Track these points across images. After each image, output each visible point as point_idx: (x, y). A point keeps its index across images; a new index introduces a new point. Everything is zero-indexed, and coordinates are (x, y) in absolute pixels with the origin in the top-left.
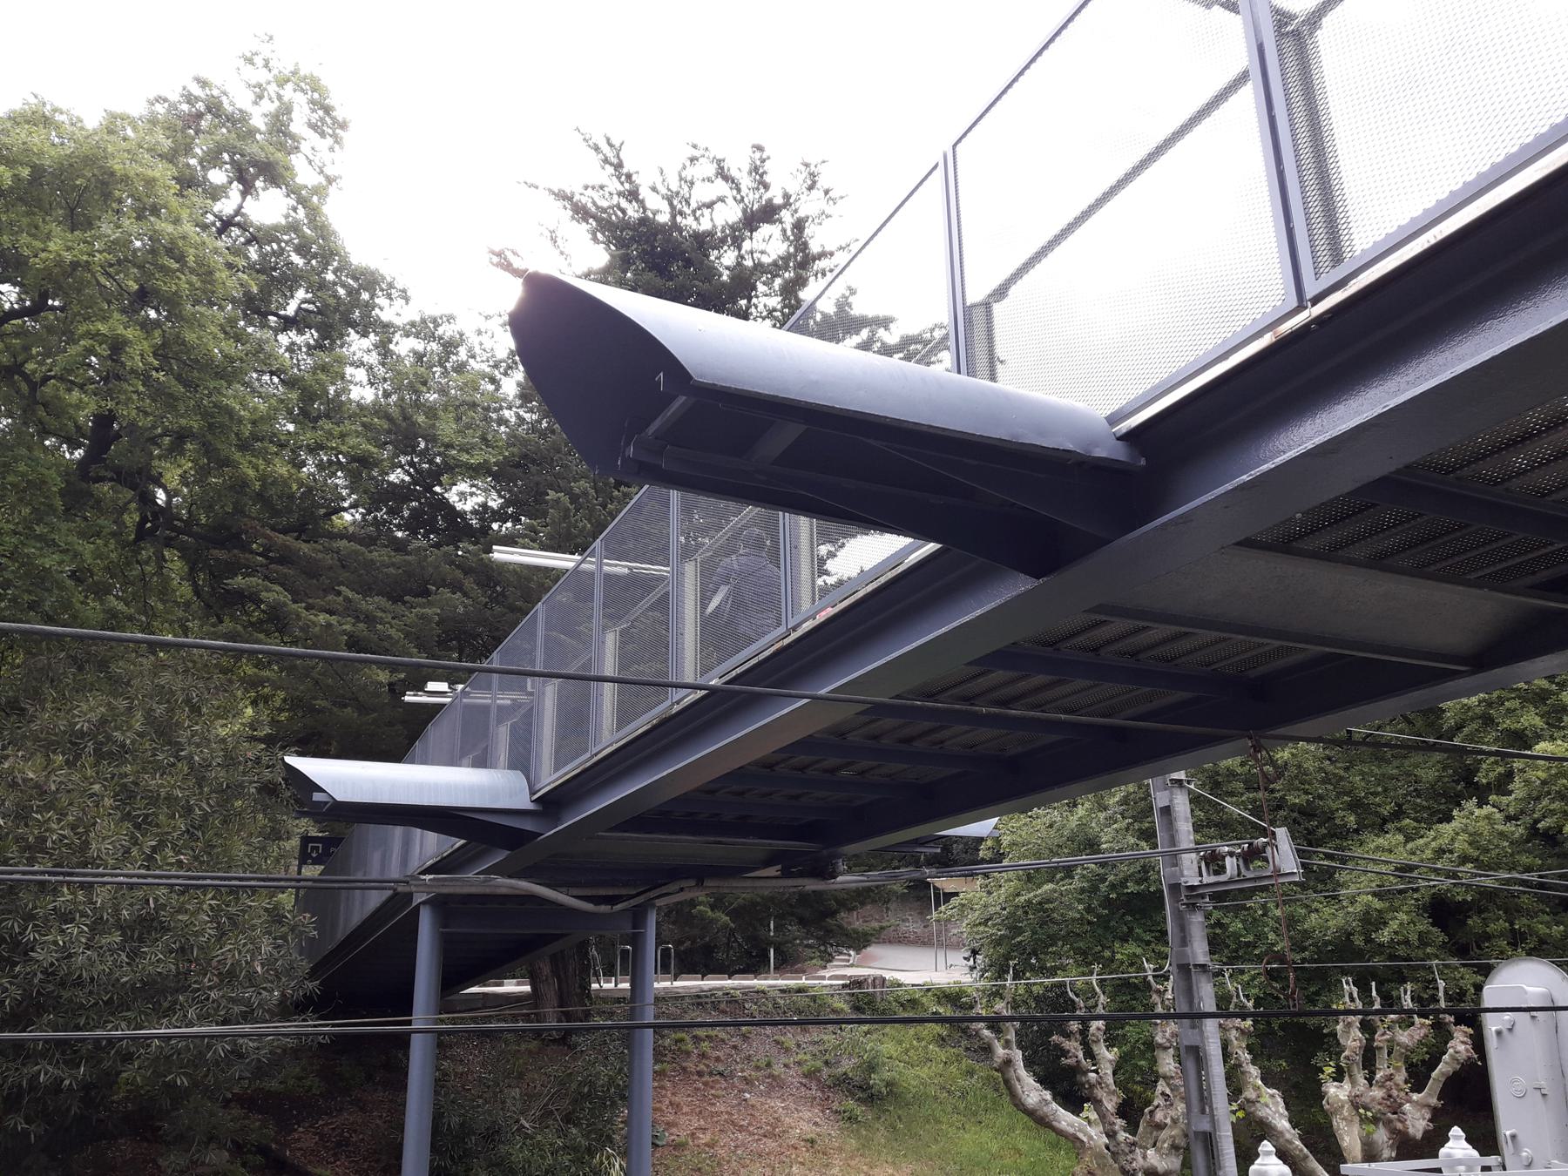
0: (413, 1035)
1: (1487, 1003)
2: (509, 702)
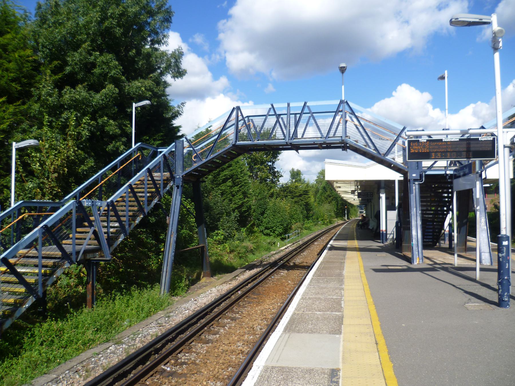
2: (72, 201)
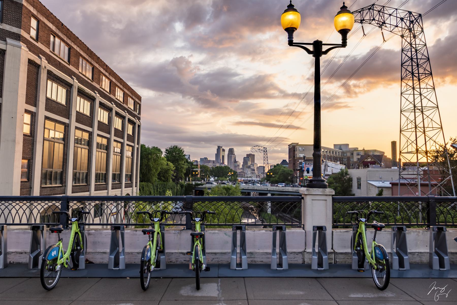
0: (165, 268)
1: (54, 137)
